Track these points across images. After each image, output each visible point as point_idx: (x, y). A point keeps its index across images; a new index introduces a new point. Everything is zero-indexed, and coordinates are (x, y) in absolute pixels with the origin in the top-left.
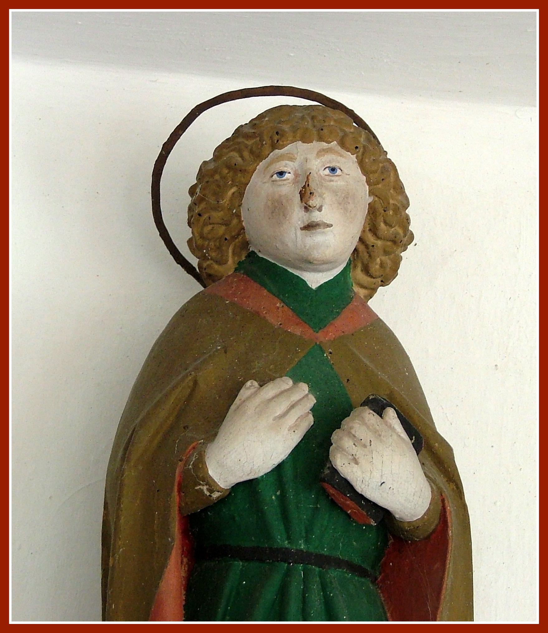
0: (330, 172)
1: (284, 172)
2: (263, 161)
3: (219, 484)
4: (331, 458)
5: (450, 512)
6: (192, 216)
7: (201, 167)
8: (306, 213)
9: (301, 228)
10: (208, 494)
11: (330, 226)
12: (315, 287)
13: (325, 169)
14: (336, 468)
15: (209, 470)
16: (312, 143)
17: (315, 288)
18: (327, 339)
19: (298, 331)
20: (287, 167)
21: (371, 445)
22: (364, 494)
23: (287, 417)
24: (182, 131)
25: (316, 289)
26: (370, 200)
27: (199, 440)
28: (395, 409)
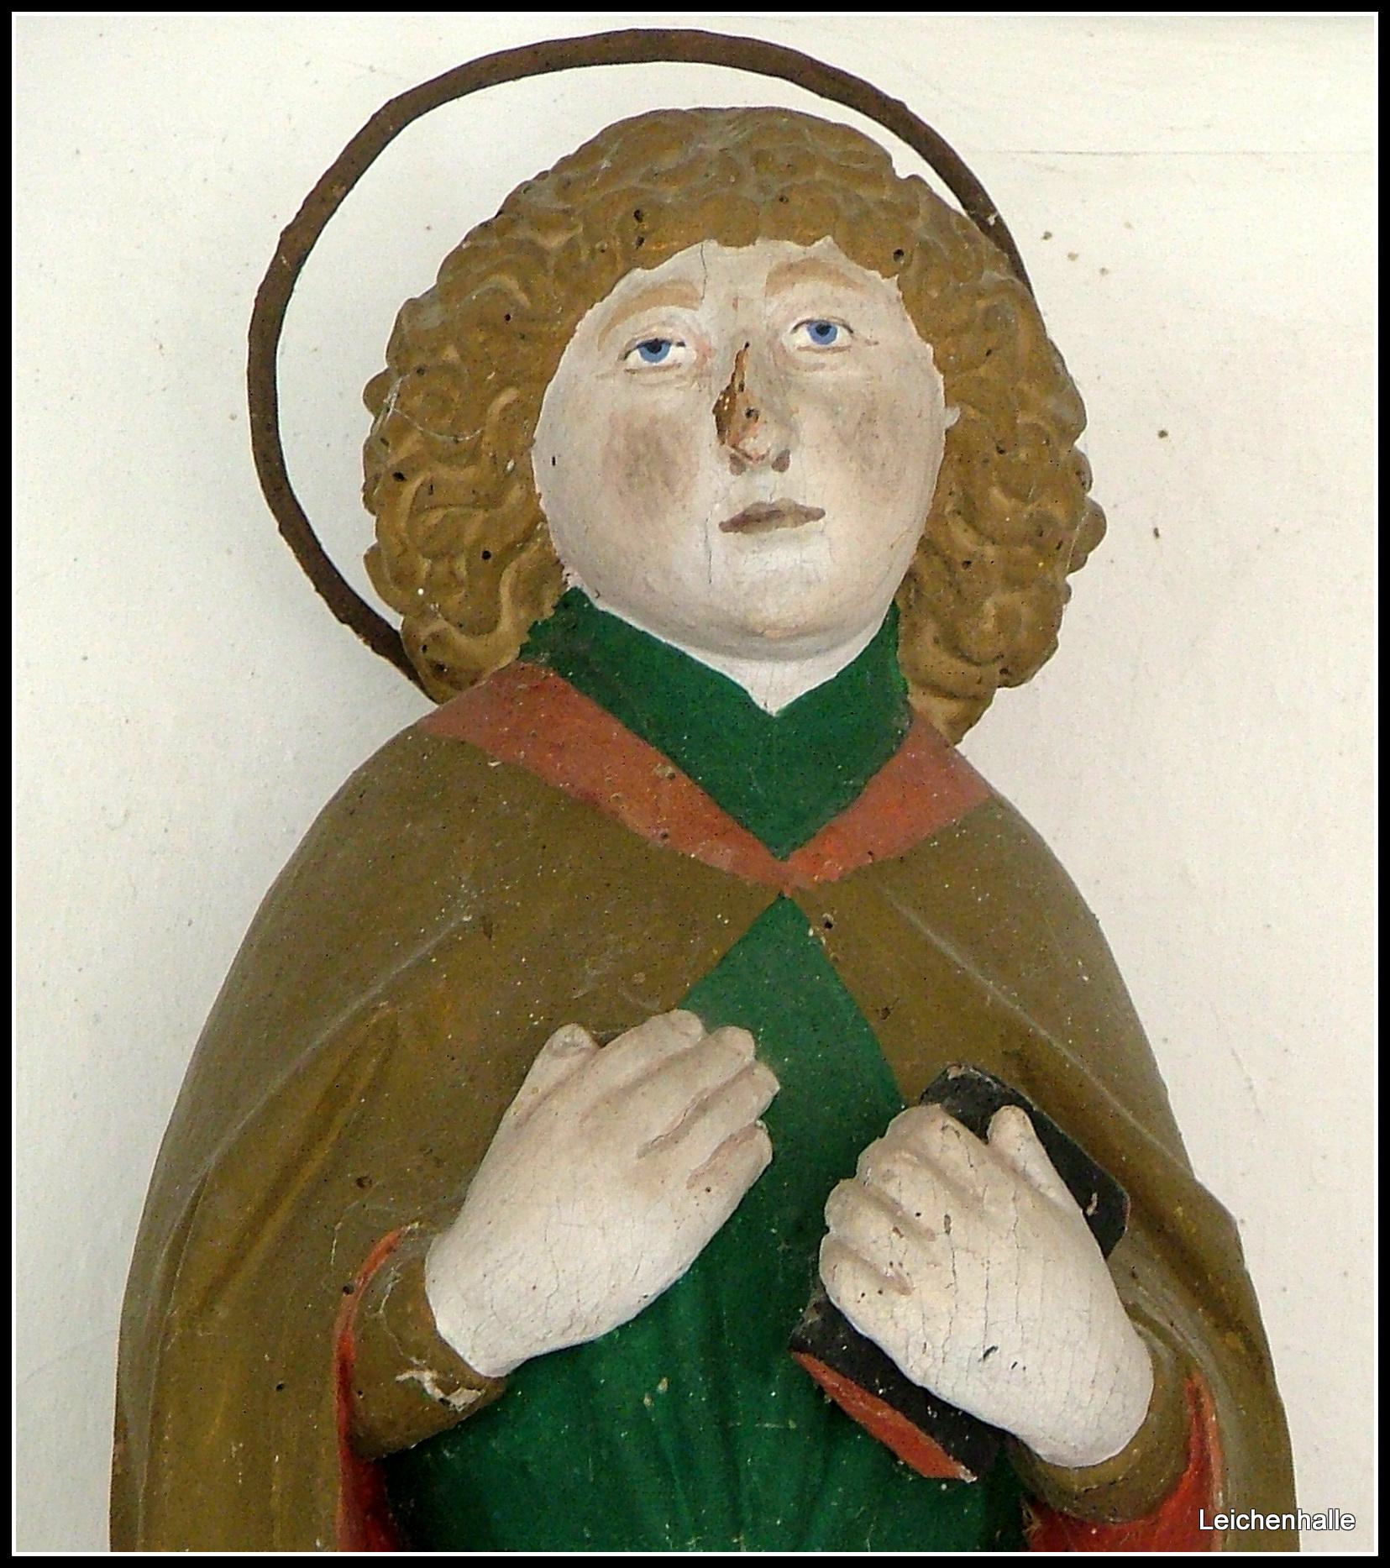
0: (814, 338)
1: (663, 342)
2: (597, 304)
3: (471, 1363)
4: (824, 1275)
5: (1220, 1433)
6: (377, 478)
7: (399, 315)
8: (734, 478)
9: (721, 524)
10: (438, 1394)
11: (816, 515)
12: (778, 708)
13: (796, 328)
14: (838, 1306)
15: (437, 1320)
16: (751, 246)
17: (777, 713)
18: (816, 878)
19: (723, 857)
20: (671, 325)
21: (948, 1232)
22: (931, 1387)
23: (682, 1146)
24: (344, 188)
25: (778, 715)
26: (951, 418)
27: (407, 1225)
28: (1028, 1110)
